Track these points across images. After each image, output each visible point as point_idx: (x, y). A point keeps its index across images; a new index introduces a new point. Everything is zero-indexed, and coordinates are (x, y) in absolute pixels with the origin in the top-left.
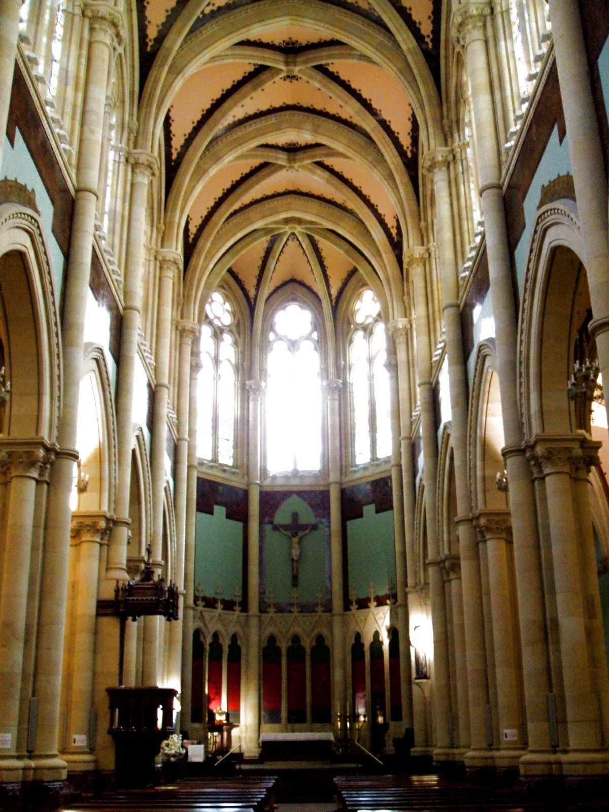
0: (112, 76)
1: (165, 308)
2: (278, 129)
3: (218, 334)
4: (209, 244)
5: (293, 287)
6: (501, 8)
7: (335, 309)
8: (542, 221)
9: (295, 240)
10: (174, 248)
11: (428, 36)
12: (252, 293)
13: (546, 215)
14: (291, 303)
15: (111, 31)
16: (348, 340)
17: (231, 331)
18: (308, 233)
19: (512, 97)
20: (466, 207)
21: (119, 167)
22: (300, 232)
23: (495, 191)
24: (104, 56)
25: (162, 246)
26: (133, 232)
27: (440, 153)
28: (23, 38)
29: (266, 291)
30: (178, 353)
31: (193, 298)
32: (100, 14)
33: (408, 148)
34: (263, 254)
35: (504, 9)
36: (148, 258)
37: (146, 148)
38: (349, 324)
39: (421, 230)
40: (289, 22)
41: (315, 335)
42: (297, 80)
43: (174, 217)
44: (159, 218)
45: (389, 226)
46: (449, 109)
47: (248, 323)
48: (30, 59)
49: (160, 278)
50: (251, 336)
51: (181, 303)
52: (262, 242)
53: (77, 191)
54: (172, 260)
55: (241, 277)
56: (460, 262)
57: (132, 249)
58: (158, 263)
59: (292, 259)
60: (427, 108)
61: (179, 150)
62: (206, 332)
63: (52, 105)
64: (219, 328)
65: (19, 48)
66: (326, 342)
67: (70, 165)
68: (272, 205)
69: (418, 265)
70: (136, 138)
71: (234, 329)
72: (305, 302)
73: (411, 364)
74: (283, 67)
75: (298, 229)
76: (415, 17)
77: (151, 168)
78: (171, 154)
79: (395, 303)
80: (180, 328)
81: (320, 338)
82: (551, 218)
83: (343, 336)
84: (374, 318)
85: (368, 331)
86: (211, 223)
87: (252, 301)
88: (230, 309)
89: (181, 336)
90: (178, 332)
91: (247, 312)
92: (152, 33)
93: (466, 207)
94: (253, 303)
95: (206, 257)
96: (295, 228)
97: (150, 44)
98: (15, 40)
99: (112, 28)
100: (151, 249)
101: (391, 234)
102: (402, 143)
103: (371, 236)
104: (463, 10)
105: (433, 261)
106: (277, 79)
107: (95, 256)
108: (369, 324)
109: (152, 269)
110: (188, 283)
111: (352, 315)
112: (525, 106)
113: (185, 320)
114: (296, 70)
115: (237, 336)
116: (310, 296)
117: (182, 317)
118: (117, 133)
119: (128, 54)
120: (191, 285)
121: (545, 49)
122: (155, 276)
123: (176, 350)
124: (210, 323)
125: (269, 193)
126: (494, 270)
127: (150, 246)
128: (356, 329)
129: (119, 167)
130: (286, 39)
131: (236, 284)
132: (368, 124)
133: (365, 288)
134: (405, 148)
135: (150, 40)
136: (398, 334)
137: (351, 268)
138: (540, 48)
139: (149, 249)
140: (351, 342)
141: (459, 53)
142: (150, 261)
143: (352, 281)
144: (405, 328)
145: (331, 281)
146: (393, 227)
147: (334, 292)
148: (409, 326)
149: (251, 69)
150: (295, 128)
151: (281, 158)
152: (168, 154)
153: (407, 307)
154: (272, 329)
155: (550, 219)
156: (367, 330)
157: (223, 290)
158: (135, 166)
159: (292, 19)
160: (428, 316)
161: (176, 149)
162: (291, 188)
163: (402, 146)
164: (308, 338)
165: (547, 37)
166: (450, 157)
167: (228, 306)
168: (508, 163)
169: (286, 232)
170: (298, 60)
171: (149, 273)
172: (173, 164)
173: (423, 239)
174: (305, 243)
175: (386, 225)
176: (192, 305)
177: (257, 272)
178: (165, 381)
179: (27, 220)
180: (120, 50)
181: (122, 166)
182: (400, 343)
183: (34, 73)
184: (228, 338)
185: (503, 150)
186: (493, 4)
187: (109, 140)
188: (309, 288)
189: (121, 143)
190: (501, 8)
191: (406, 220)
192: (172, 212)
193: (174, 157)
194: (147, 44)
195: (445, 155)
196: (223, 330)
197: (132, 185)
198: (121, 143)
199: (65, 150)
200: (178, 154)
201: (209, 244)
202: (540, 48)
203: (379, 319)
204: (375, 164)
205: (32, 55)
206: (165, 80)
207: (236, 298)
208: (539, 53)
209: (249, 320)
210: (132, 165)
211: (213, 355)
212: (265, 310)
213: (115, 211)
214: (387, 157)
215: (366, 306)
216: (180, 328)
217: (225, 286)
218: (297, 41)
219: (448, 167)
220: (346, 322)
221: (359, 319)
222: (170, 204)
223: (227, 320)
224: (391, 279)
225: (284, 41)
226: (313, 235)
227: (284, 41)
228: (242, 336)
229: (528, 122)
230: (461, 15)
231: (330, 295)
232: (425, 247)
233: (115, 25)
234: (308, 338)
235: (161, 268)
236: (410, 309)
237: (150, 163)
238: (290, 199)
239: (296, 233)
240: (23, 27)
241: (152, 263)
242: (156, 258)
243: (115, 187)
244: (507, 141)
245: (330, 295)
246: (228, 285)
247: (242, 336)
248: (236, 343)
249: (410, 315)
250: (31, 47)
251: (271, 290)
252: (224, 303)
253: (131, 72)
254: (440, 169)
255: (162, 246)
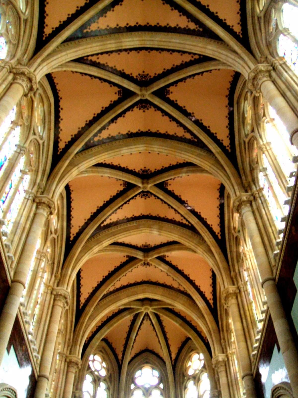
0: (62, 319)
1: (53, 324)
2: (138, 228)
3: (96, 381)
4: (92, 309)
5: (147, 355)
6: (244, 289)
7: (174, 367)
8: (275, 393)
9: (148, 320)
10: (77, 355)
11: (228, 146)
12: (120, 357)
13: (278, 389)
14: (145, 365)
15: (63, 301)
16: (183, 388)
17: (105, 380)
18: (156, 312)
19: (273, 232)
20: (268, 220)
21: (27, 202)
22: (151, 312)
23: (270, 282)
24: (59, 311)
25: (58, 286)
26: (30, 238)
27: (232, 289)
28: (21, 304)
29: (128, 357)
30: (64, 377)
31: (79, 342)
32: (59, 293)
33: (218, 233)
34: (127, 329)
35: (245, 290)
36: (46, 291)
37: (75, 354)
38: (184, 376)
39: (232, 278)
40: (144, 148)
41: (161, 386)
42: (149, 266)
43: (68, 271)
44: (57, 271)
45: (208, 299)
46: (246, 177)
47: (116, 375)
48: (24, 313)
49: (53, 306)
50: (119, 384)
51: (71, 345)
52: (127, 318)
53: (13, 282)
54: (75, 361)
55: (114, 346)
56: (270, 252)
57: (26, 248)
58: (53, 296)
59: (146, 335)
60: (232, 178)
61: (75, 235)
62: (88, 378)
63: (32, 334)
64: (97, 376)
65: (19, 308)
66: (169, 389)
67: (11, 267)
68: (133, 290)
69: (232, 298)
70: (71, 349)
71: (108, 380)
72: (155, 364)
73: (230, 385)
74: (140, 185)
75: (150, 310)
76: (219, 137)
77: (50, 207)
78: (70, 237)
79: (216, 346)
80: (68, 360)
81: (164, 386)
82: (278, 392)
83: (180, 384)
84: (199, 370)
85: (197, 379)
86: (94, 298)
87: (120, 362)
88: (105, 366)
89: (68, 367)
90: (66, 363)
91: (116, 368)
92: (83, 300)
93: (268, 220)
94: (121, 363)
95: (89, 318)
96: (148, 309)
97: (60, 151)
98: (18, 305)
99: (49, 209)
100: (49, 286)
101: (210, 304)
102: (215, 231)
103: (197, 305)
104: (226, 291)
105: (243, 294)
106: (139, 264)
107: (17, 322)
108: (197, 374)
109: (48, 299)
110: (77, 332)
111: (186, 370)
112: (282, 235)
113: (72, 355)
114: (149, 259)
115: (109, 384)
116: (159, 360)
117: (70, 353)
118: (62, 347)
119: (71, 310)
120: (79, 334)
121: (265, 308)
122: (49, 304)
123: (63, 375)
124: (92, 373)
125: (132, 282)
126: (279, 327)
127: (48, 284)
128: (189, 379)
129: (27, 202)
130: (144, 244)
131: (110, 351)
132: (194, 221)
133: (193, 352)
134: (217, 234)
135: (60, 149)
136: (220, 365)
137: (184, 339)
138: (263, 307)
139: (47, 286)
140: (185, 388)
141: (226, 309)
142: (47, 293)
143: (185, 349)
144: (224, 361)
145: (172, 349)
146: (210, 299)
147: (174, 356)
148: (226, 359)
149: (125, 259)
150: (148, 227)
151: (139, 255)
152: (68, 237)
153: (224, 347)
154: (133, 381)
155: (282, 392)
156: (196, 379)
157: (101, 354)
158: (39, 204)
159: (145, 147)
160: (244, 329)
161: (73, 235)
162: (146, 279)
163: (215, 233)
164: (157, 387)
165: (264, 303)
166: (252, 198)
167: (104, 364)
168: (255, 362)
169: (142, 312)
170: (150, 181)
171: (45, 300)
172: (70, 243)
173: (223, 350)
174: (154, 321)
175: (206, 298)
176: (78, 347)
177: (124, 342)
178: (47, 373)
179: (10, 392)
180: (67, 308)
181: (29, 202)
182: (221, 371)
183: (24, 320)
184: (103, 386)
185: (251, 356)
186: (240, 288)
187: (58, 350)
188: (157, 355)
189: (32, 189)
190: (244, 289)
191: (213, 342)
192: (66, 269)
193: (72, 239)
194: (80, 305)
195: (249, 197)
196: (100, 378)
197: (35, 214)
198: (32, 189)
199: (35, 356)
200: (74, 237)
201: (92, 309)
202: (263, 307)
203: (204, 370)
204: (199, 244)
205: (25, 311)
206: (87, 322)
207: (109, 359)
208: (263, 309)
209: (118, 374)
210: (68, 362)
211: (92, 394)
212: (128, 369)
213: (19, 223)
214: (206, 239)
215: (196, 363)
216: (68, 360)
217: (103, 351)
218: (149, 245)
219: (251, 205)
220: (181, 375)
221: (191, 372)
222: (66, 264)
223: (103, 373)
224: (212, 330)
225: (143, 245)
226: (159, 313)
227: (143, 245)
228: (113, 384)
229: (262, 342)
230: (238, 201)
231: (171, 358)
232: (236, 286)
233: (66, 298)
234: (157, 387)
235: (55, 300)
236: (226, 348)
237: (78, 362)
238: (145, 286)
239: (149, 312)
240: (22, 300)
241: (49, 295)
242: (51, 293)
243: (22, 211)
244: (253, 351)
245: (171, 358)
246: (105, 350)
247: (113, 384)
248: (108, 389)
249: (227, 351)
250: (24, 308)
251: (133, 355)
252: (102, 362)
253: (72, 317)
254: (246, 206)
255: (58, 286)
